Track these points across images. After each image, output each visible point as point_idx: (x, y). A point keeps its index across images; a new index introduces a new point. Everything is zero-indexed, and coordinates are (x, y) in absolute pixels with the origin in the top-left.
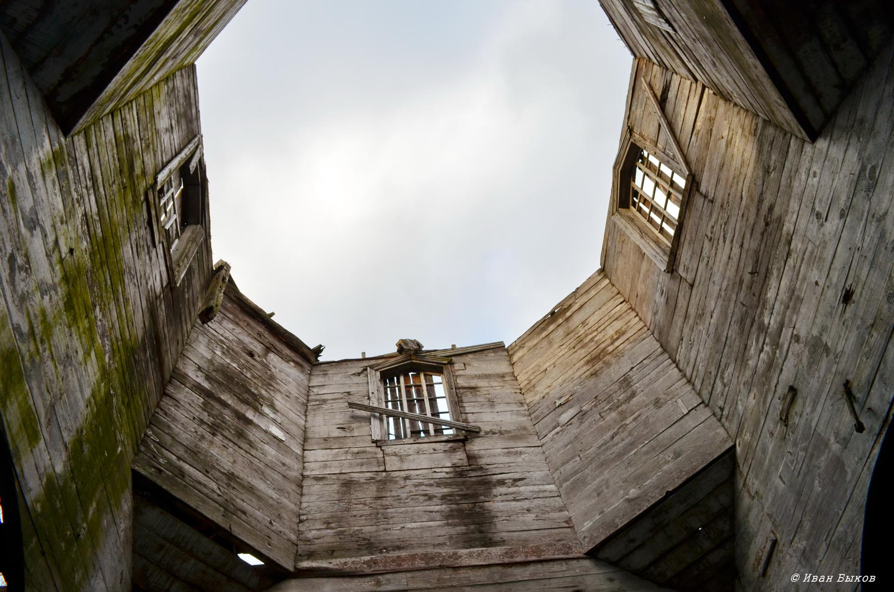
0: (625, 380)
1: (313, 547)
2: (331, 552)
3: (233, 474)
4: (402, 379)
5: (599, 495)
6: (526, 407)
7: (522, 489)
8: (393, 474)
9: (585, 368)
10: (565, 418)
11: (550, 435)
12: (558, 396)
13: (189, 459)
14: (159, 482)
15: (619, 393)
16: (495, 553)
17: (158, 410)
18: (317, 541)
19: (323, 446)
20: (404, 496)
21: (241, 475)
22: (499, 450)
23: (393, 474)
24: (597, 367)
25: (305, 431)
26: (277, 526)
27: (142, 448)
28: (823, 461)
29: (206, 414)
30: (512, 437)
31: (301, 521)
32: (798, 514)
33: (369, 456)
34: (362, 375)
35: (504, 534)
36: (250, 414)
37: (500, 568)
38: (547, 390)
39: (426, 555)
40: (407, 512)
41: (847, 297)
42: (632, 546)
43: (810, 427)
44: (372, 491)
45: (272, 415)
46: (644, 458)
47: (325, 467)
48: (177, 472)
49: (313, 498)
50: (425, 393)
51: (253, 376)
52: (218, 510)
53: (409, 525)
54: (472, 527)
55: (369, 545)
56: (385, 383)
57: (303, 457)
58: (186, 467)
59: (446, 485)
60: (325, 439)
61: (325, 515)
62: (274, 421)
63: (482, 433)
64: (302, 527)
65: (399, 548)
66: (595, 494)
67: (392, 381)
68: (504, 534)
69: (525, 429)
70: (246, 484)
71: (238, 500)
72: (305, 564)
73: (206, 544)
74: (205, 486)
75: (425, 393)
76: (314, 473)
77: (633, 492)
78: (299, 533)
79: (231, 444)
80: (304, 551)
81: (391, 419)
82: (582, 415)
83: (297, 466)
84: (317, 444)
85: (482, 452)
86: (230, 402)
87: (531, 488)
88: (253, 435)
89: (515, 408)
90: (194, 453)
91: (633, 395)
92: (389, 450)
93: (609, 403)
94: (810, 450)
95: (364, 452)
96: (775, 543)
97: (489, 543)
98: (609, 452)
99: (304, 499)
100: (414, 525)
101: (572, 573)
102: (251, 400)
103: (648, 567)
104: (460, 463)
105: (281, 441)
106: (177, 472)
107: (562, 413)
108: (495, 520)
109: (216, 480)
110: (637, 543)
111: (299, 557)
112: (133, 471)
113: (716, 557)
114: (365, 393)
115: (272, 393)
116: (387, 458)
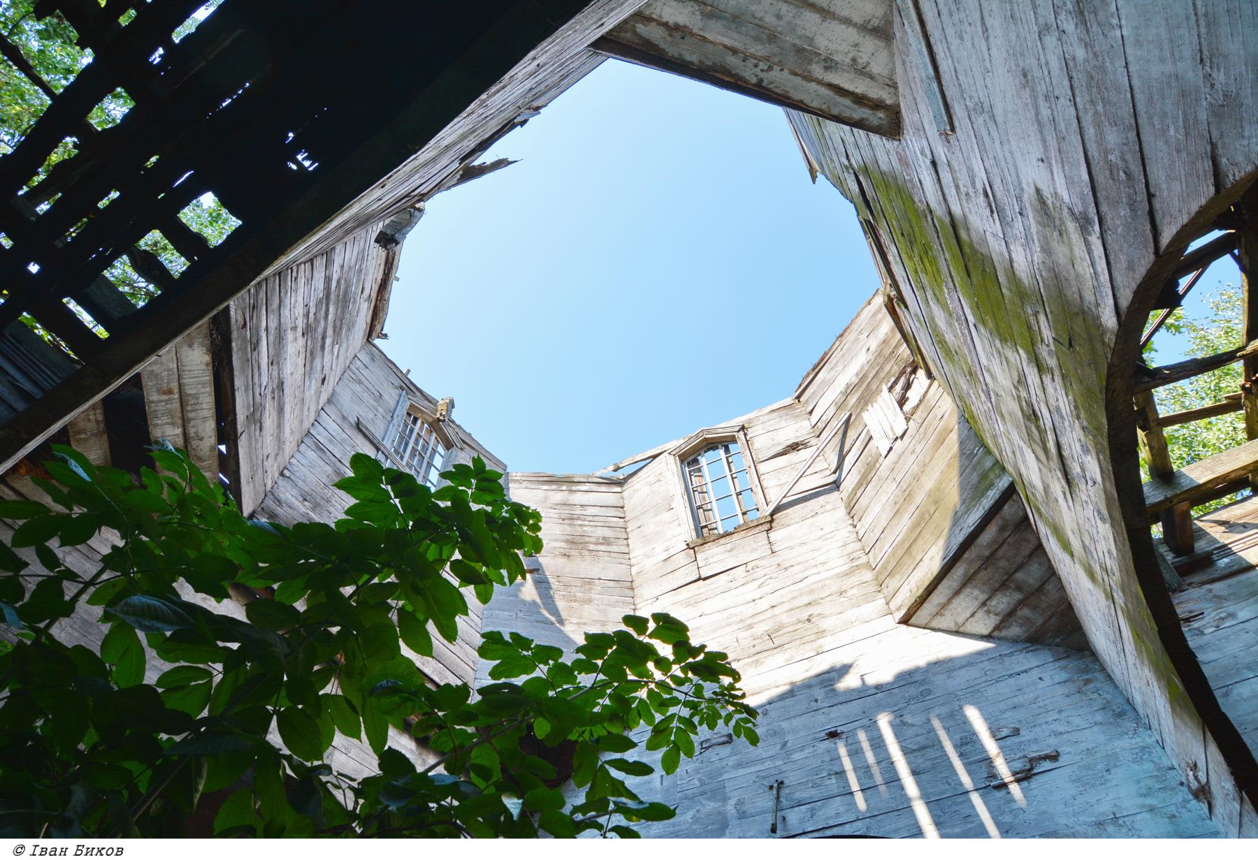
13: (271, 338)
14: (235, 335)
18: (286, 508)
43: (721, 775)
48: (254, 340)
61: (306, 489)
80: (268, 507)
94: (707, 787)
106: (254, 340)
109: (270, 377)
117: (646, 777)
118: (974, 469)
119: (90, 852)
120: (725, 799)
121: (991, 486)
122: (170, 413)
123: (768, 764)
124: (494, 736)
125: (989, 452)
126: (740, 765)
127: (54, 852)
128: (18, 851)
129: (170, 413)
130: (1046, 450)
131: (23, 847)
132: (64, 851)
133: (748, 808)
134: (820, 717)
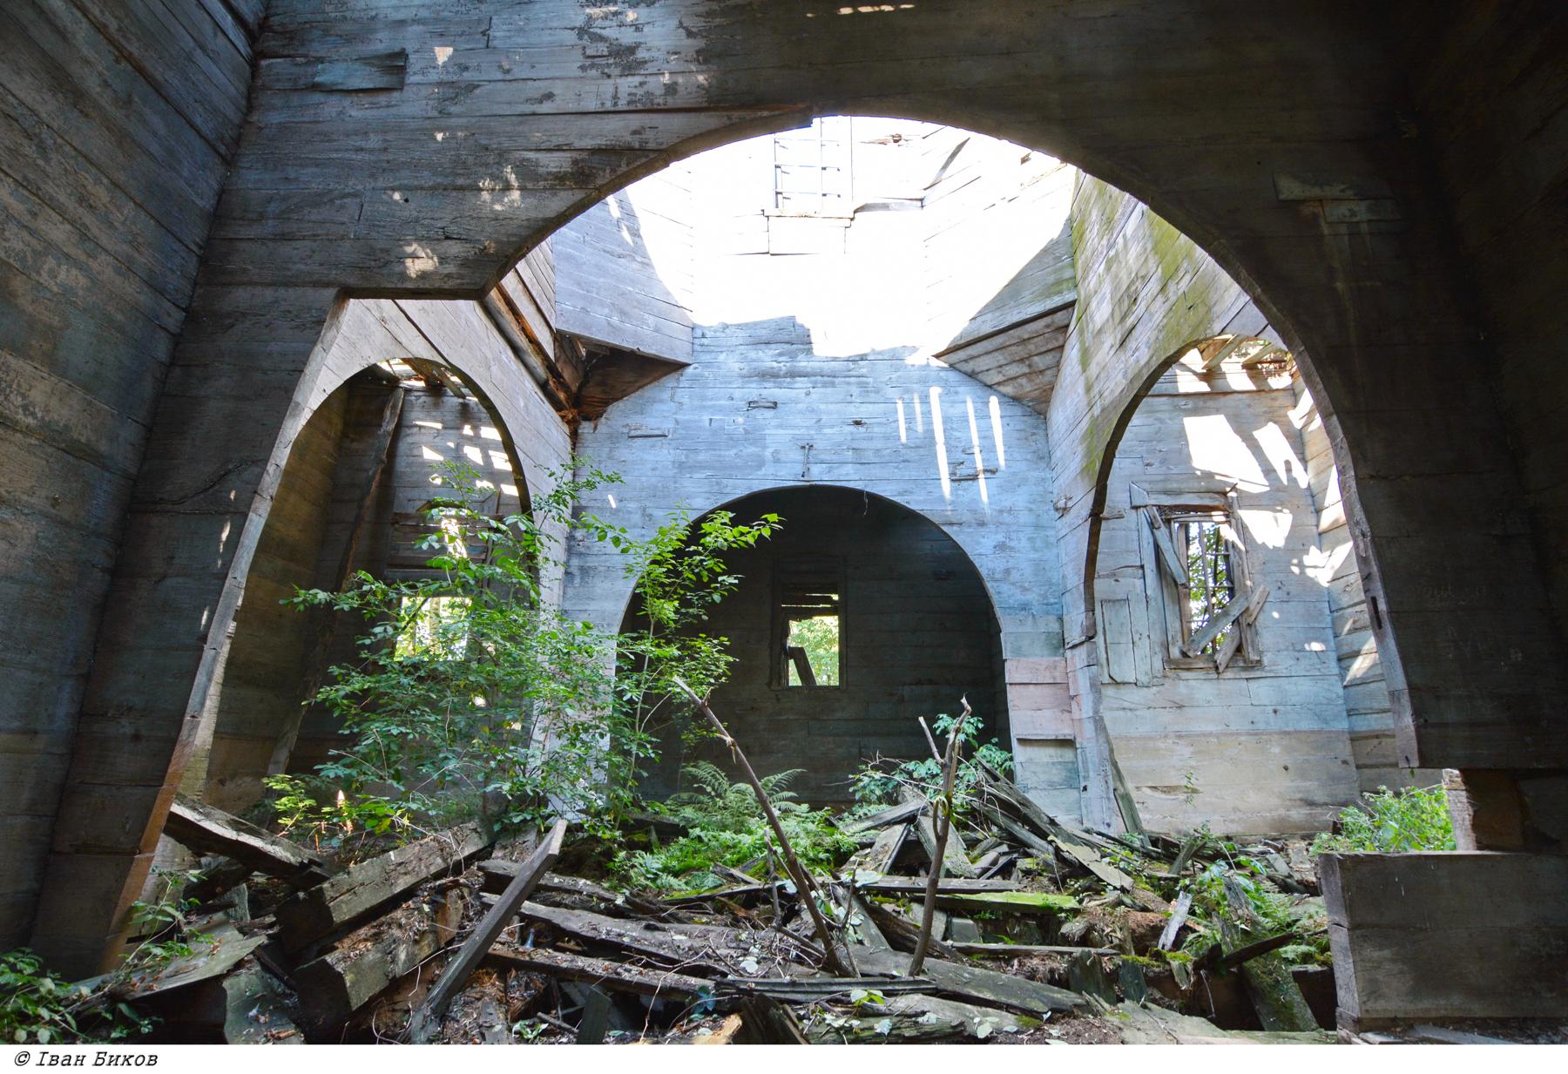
28: (752, 449)
41: (858, 423)
77: (615, 320)
118: (1055, 272)
119: (114, 1061)
120: (764, 447)
121: (1060, 292)
123: (803, 431)
125: (1073, 265)
126: (780, 426)
127: (67, 1061)
128: (21, 1060)
130: (1123, 319)
131: (27, 1054)
132: (80, 1060)
133: (782, 457)
134: (851, 408)
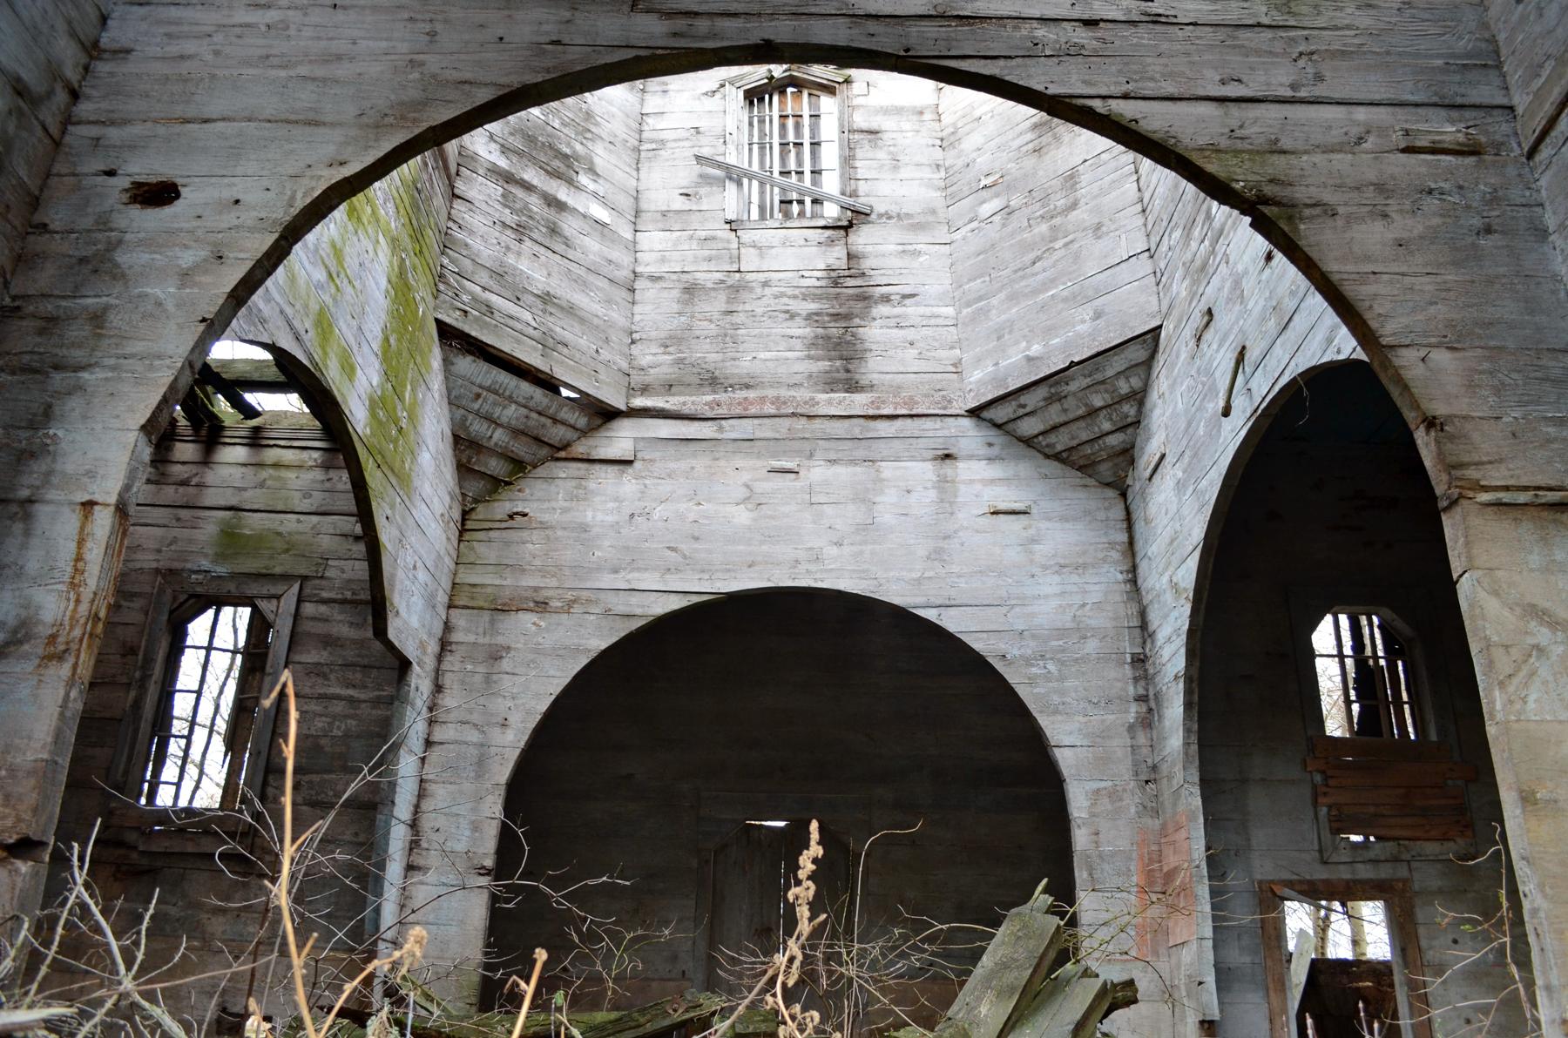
0: (1072, 177)
1: (648, 380)
2: (669, 387)
3: (548, 294)
4: (776, 98)
5: (999, 339)
6: (943, 174)
7: (910, 310)
8: (749, 277)
9: (1030, 136)
10: (987, 209)
11: (963, 231)
12: (986, 170)
13: (496, 287)
14: (467, 329)
15: (1058, 196)
16: (860, 402)
17: (451, 224)
19: (661, 226)
20: (759, 311)
21: (559, 293)
22: (892, 247)
23: (749, 277)
24: (1044, 140)
25: (636, 199)
26: (605, 354)
27: (442, 287)
29: (507, 211)
30: (912, 225)
31: (633, 342)
32: (1184, 443)
33: (720, 246)
34: (718, 95)
35: (875, 376)
36: (563, 194)
37: (862, 421)
38: (974, 155)
39: (778, 398)
40: (761, 336)
42: (1021, 411)
44: (719, 303)
45: (592, 186)
46: (1061, 306)
47: (663, 260)
49: (648, 308)
50: (806, 131)
51: (564, 124)
52: (535, 349)
53: (762, 355)
54: (838, 363)
55: (713, 381)
56: (751, 103)
57: (635, 242)
58: (494, 298)
59: (817, 298)
60: (664, 214)
62: (595, 195)
63: (873, 216)
64: (635, 350)
65: (748, 387)
66: (994, 337)
67: (761, 100)
68: (875, 376)
69: (933, 212)
70: (564, 304)
71: (558, 329)
72: (639, 402)
73: (526, 388)
74: (518, 320)
75: (806, 131)
76: (648, 269)
77: (1036, 349)
78: (631, 358)
79: (543, 250)
81: (755, 183)
82: (1008, 211)
83: (625, 259)
84: (655, 221)
85: (869, 248)
86: (535, 182)
87: (922, 310)
88: (569, 225)
89: (927, 173)
90: (499, 274)
91: (1074, 206)
92: (746, 236)
93: (1043, 206)
95: (714, 238)
96: (1163, 456)
97: (853, 387)
98: (1023, 283)
99: (637, 309)
100: (768, 355)
101: (946, 433)
102: (563, 168)
103: (1036, 436)
104: (836, 264)
105: (604, 225)
107: (984, 202)
108: (868, 355)
109: (529, 308)
110: (1028, 409)
111: (631, 390)
112: (437, 320)
113: (1114, 440)
114: (719, 131)
115: (589, 144)
116: (743, 250)
117: (502, 772)
122: (495, 404)
124: (162, 591)
129: (495, 404)
